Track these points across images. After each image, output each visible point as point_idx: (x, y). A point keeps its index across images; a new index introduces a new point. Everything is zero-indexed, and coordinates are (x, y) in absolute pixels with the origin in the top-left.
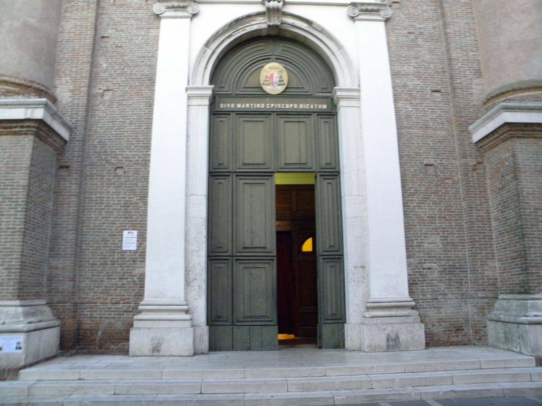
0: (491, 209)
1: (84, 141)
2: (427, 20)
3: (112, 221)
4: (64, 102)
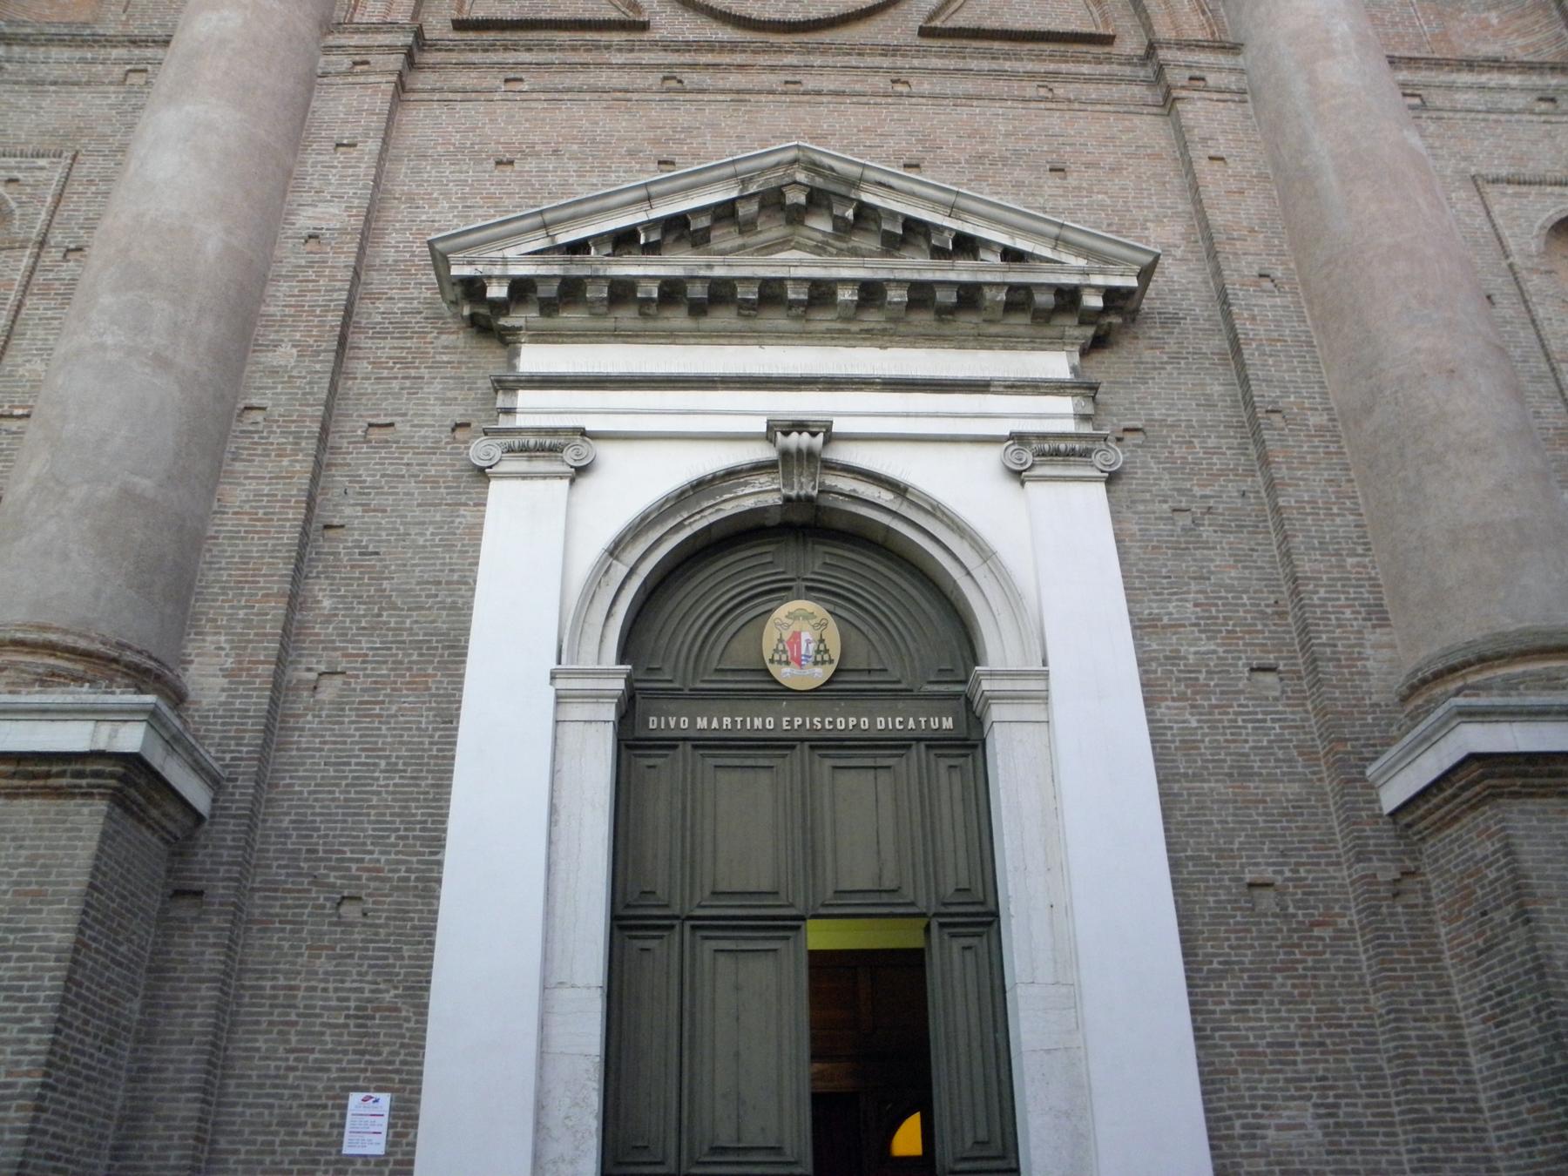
0: (1462, 1015)
1: (251, 820)
2: (1222, 473)
3: (316, 1060)
4: (205, 703)
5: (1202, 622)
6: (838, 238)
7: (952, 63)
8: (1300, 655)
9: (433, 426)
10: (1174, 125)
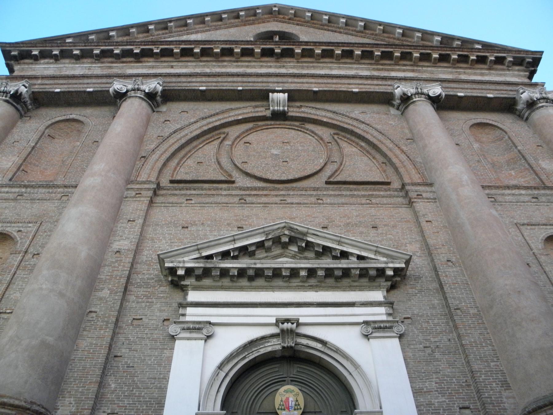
2: (441, 332)
5: (439, 390)
6: (300, 253)
7: (337, 193)
8: (478, 402)
9: (156, 320)
10: (413, 211)
